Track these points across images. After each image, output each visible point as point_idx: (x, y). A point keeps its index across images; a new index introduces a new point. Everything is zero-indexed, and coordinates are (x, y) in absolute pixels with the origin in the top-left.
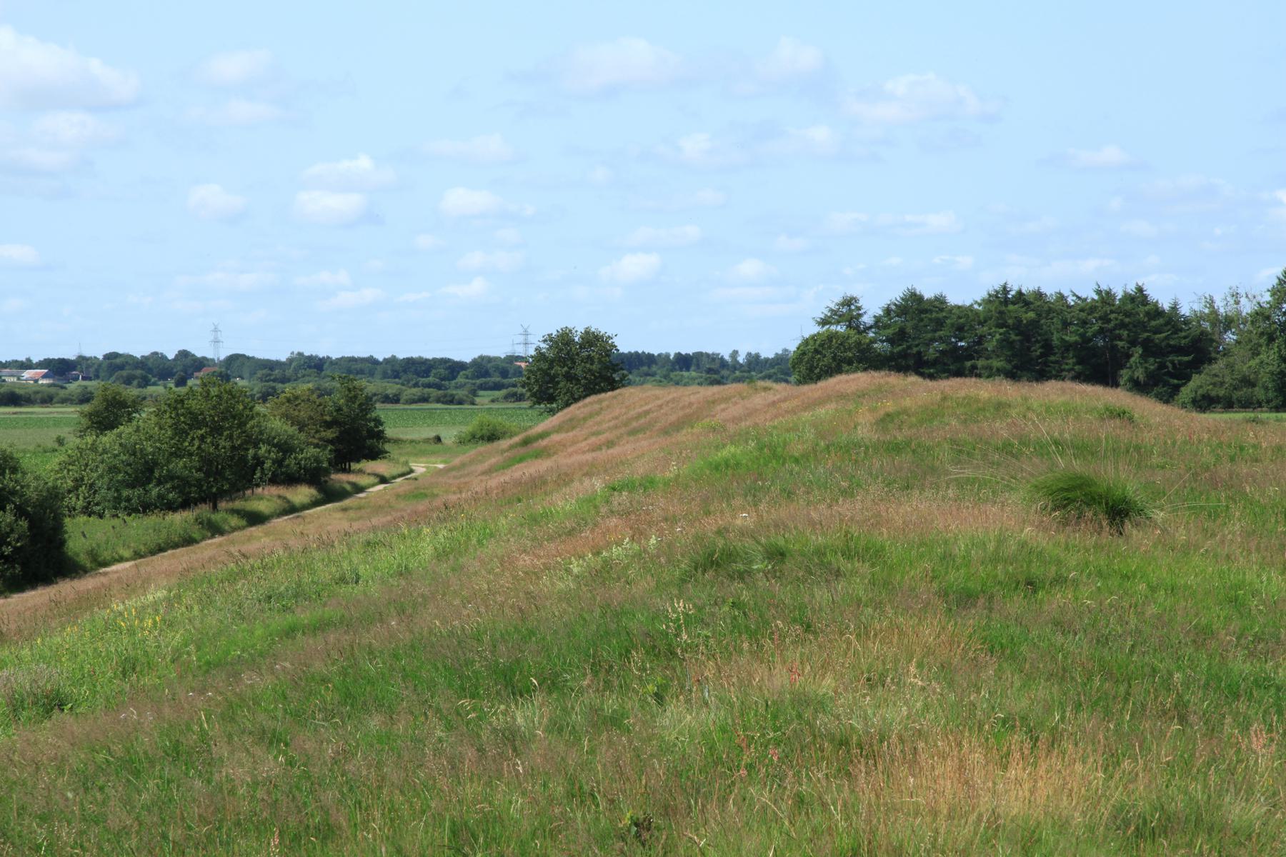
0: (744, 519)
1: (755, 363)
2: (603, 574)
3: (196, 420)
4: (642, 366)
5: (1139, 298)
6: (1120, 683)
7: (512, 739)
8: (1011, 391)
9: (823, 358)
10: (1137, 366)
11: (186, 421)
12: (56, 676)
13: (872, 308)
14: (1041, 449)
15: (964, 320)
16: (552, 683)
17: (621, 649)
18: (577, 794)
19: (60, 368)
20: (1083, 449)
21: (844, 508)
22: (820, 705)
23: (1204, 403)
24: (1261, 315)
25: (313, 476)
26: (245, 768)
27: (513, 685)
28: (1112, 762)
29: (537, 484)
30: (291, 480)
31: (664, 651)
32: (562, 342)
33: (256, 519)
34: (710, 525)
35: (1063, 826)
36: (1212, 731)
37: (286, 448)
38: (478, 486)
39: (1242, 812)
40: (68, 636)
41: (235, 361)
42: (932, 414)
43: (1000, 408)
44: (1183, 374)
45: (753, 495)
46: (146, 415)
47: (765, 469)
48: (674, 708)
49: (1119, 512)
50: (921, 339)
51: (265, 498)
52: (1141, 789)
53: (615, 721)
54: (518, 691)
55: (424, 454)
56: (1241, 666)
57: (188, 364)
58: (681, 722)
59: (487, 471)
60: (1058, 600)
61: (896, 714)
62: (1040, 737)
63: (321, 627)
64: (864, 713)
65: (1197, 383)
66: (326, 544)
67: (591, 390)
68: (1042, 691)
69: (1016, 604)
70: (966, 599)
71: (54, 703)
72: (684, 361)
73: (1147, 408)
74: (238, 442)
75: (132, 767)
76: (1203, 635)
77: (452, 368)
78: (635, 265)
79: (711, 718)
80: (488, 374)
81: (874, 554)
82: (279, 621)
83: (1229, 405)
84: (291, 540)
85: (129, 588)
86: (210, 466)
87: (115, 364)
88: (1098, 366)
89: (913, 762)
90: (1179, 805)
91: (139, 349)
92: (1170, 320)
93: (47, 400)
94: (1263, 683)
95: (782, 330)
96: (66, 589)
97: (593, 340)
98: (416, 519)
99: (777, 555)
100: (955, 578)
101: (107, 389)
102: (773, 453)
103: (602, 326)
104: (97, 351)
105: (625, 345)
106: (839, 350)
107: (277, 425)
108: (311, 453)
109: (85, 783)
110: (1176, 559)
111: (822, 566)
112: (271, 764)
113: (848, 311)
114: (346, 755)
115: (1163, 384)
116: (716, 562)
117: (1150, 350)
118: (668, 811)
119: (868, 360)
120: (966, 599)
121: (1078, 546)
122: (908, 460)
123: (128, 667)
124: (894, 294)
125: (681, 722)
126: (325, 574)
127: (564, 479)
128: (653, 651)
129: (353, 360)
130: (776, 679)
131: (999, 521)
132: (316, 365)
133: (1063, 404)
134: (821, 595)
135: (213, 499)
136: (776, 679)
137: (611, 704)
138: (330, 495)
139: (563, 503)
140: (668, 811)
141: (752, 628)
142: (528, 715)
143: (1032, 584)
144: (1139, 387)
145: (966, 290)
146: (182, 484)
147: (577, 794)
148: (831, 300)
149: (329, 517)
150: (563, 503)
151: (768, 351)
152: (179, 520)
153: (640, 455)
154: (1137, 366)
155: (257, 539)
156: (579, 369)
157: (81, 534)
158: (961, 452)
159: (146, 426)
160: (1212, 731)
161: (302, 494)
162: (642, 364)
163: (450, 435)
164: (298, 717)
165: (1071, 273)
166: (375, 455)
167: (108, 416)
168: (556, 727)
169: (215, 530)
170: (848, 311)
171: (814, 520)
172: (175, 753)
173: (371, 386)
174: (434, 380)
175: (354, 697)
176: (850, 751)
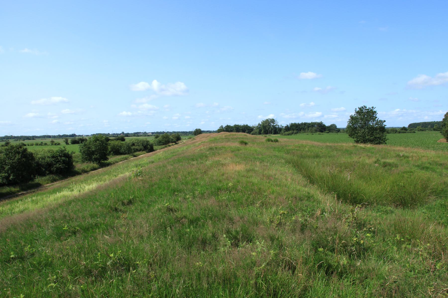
0: (213, 145)
1: (214, 131)
2: (201, 150)
3: (164, 137)
4: (204, 132)
5: (247, 125)
6: (246, 159)
7: (193, 165)
8: (237, 133)
9: (220, 130)
10: (247, 131)
11: (164, 137)
12: (153, 160)
13: (224, 126)
14: (239, 138)
15: (232, 127)
16: (197, 160)
17: (202, 157)
18: (199, 169)
19: (153, 133)
20: (243, 138)
21: (222, 144)
22: (220, 161)
23: (253, 134)
24: (257, 126)
25: (175, 142)
26: (170, 167)
27: (193, 160)
28: (246, 165)
29: (195, 142)
30: (173, 142)
31: (206, 157)
32: (197, 130)
33: (170, 146)
34: (210, 146)
35: (241, 171)
36: (254, 162)
37: (172, 140)
38: (189, 143)
39: (257, 169)
40: (154, 156)
41: (168, 132)
42: (229, 136)
43: (235, 135)
44: (251, 132)
45: (214, 143)
46: (160, 137)
47: (215, 140)
48: (207, 162)
49: (246, 144)
50: (228, 129)
51: (170, 144)
52: (248, 167)
53: (202, 163)
54: (194, 160)
55: (184, 140)
56: (256, 157)
57: (164, 132)
58: (208, 163)
59: (190, 141)
60: (241, 151)
61: (227, 162)
62: (239, 163)
63: (176, 155)
64: (223, 162)
65: (252, 132)
66: (176, 148)
67: (199, 134)
68: (240, 159)
69: (237, 152)
70: (233, 151)
71: (153, 162)
72: (207, 131)
73: (248, 135)
74: (168, 139)
75: (160, 168)
76: (253, 154)
77: (187, 132)
78: (203, 123)
79: (211, 162)
80: (190, 133)
81: (225, 148)
82: (172, 155)
83: (255, 134)
84: (173, 148)
85: (159, 152)
86: (166, 141)
87: (157, 133)
88: (244, 131)
89: (228, 166)
90: (251, 169)
91: (159, 131)
92: (250, 127)
93: (151, 136)
94: (258, 158)
95: (216, 128)
96: (154, 152)
97: (199, 129)
98: (184, 146)
99: (216, 148)
100: (232, 150)
101: (157, 135)
102: (216, 139)
103: (200, 128)
104: (156, 131)
105: (202, 130)
106: (221, 130)
107: (171, 137)
108: (175, 140)
109: (156, 169)
110: (251, 148)
111: (220, 149)
112: (172, 167)
113: (222, 127)
114: (178, 167)
115: (249, 133)
116: (211, 149)
117: (248, 130)
118: (207, 170)
119: (224, 131)
120: (233, 151)
121: (242, 147)
122: (227, 139)
123: (159, 159)
124: (226, 125)
125: (208, 163)
126: (176, 150)
127: (197, 142)
128: (205, 157)
129: (415, 123)
130: (216, 159)
131: (236, 145)
132: (175, 132)
133: (241, 134)
134: (220, 152)
135: (166, 144)
136: (216, 159)
137: (202, 161)
138: (176, 144)
139: (197, 144)
140: (207, 170)
141: (214, 154)
142: (194, 163)
143: (239, 150)
144: (247, 133)
145: (232, 125)
146: (163, 143)
147: (199, 169)
148: (220, 126)
149: (176, 146)
150: (197, 144)
151: (215, 130)
152: (163, 146)
153: (204, 139)
154: (247, 131)
155: (170, 148)
156: (198, 132)
157: (155, 147)
158: (232, 139)
159: (160, 138)
160: (254, 162)
161: (174, 144)
162: (204, 132)
163: (187, 138)
164: (174, 163)
165: (241, 123)
166: (180, 140)
167: (157, 137)
168: (197, 164)
169: (166, 147)
170: (222, 127)
171: (220, 145)
172: (163, 166)
173: (180, 134)
174: (185, 133)
175: (179, 161)
176: (223, 165)
